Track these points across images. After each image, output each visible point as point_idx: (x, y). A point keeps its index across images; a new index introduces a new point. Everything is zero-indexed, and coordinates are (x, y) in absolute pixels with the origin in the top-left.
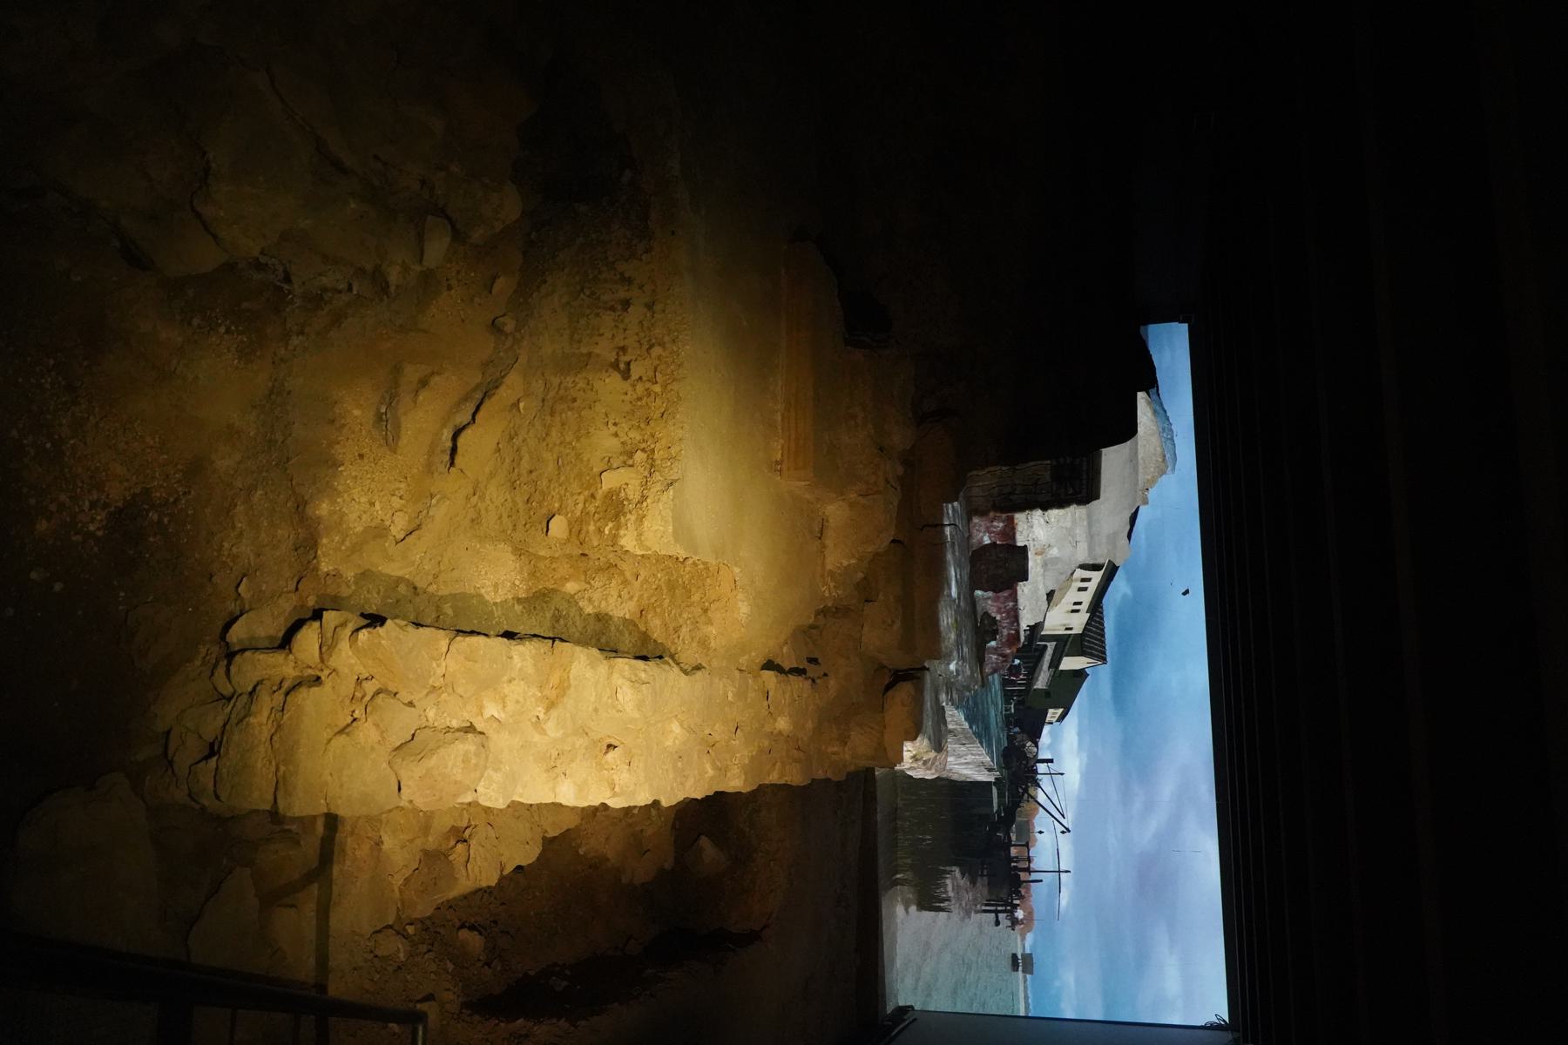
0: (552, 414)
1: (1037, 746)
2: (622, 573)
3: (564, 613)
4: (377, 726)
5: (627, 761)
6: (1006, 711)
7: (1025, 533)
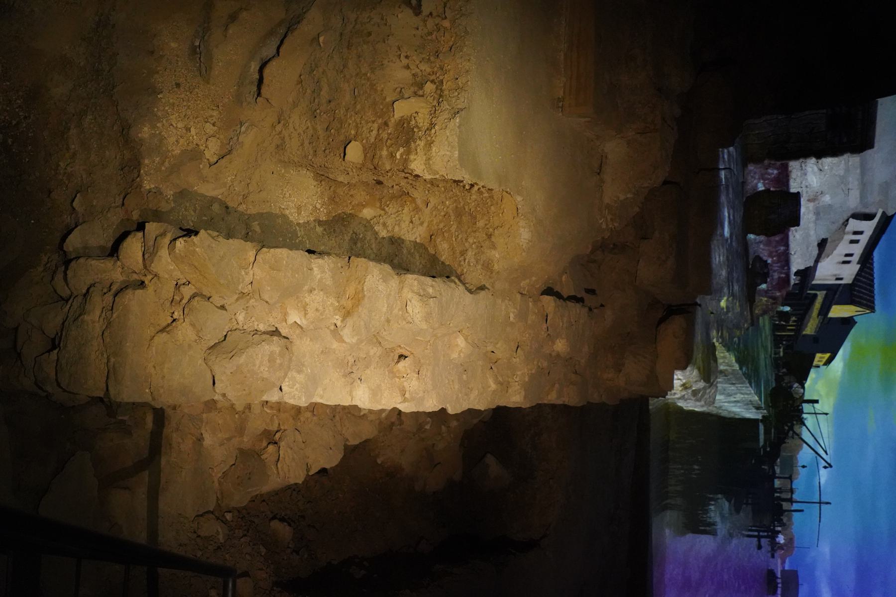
0: (349, 47)
1: (803, 388)
2: (414, 200)
3: (361, 237)
4: (193, 325)
5: (417, 370)
6: (775, 354)
7: (798, 180)
